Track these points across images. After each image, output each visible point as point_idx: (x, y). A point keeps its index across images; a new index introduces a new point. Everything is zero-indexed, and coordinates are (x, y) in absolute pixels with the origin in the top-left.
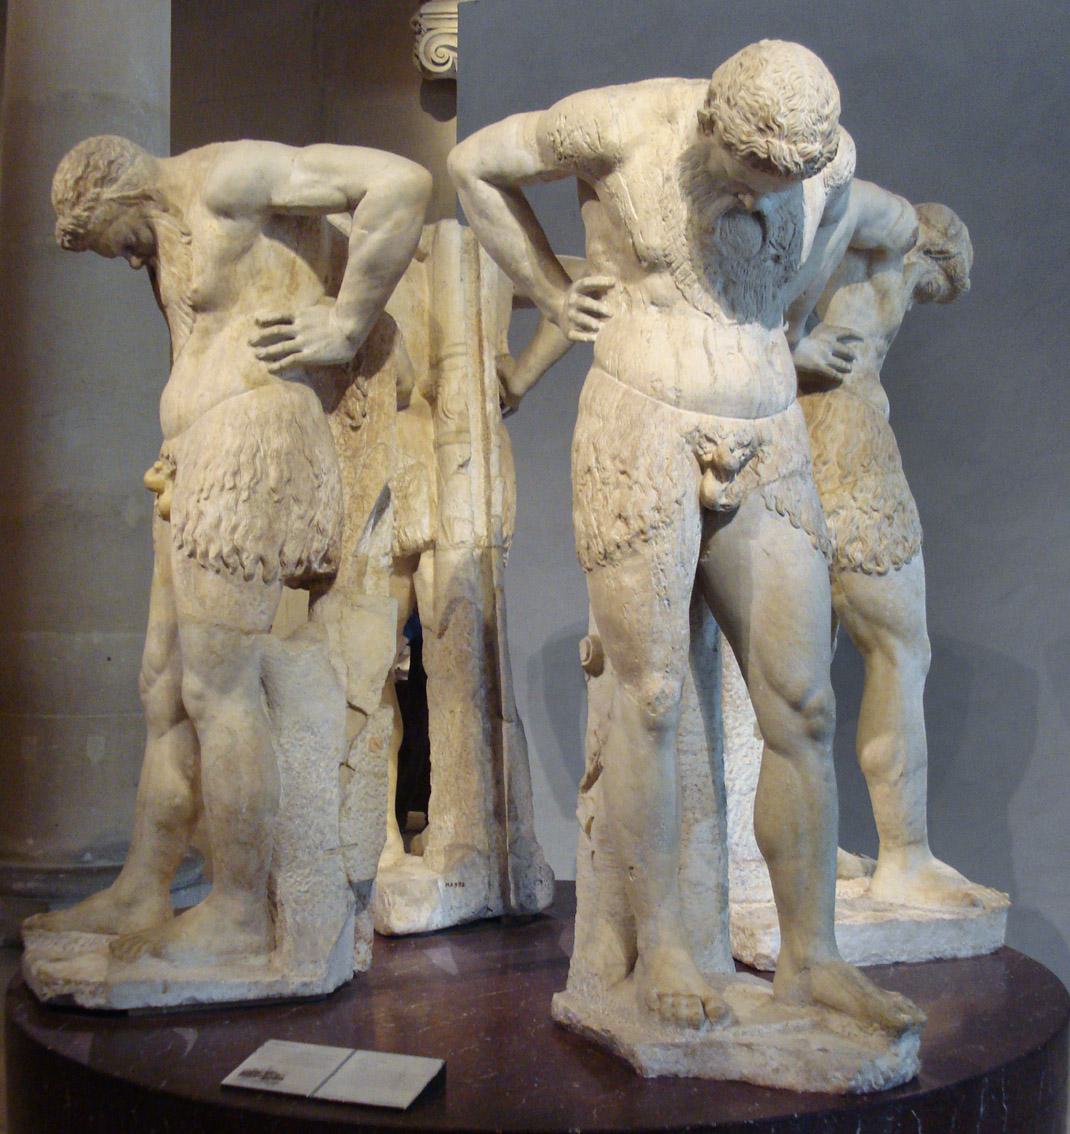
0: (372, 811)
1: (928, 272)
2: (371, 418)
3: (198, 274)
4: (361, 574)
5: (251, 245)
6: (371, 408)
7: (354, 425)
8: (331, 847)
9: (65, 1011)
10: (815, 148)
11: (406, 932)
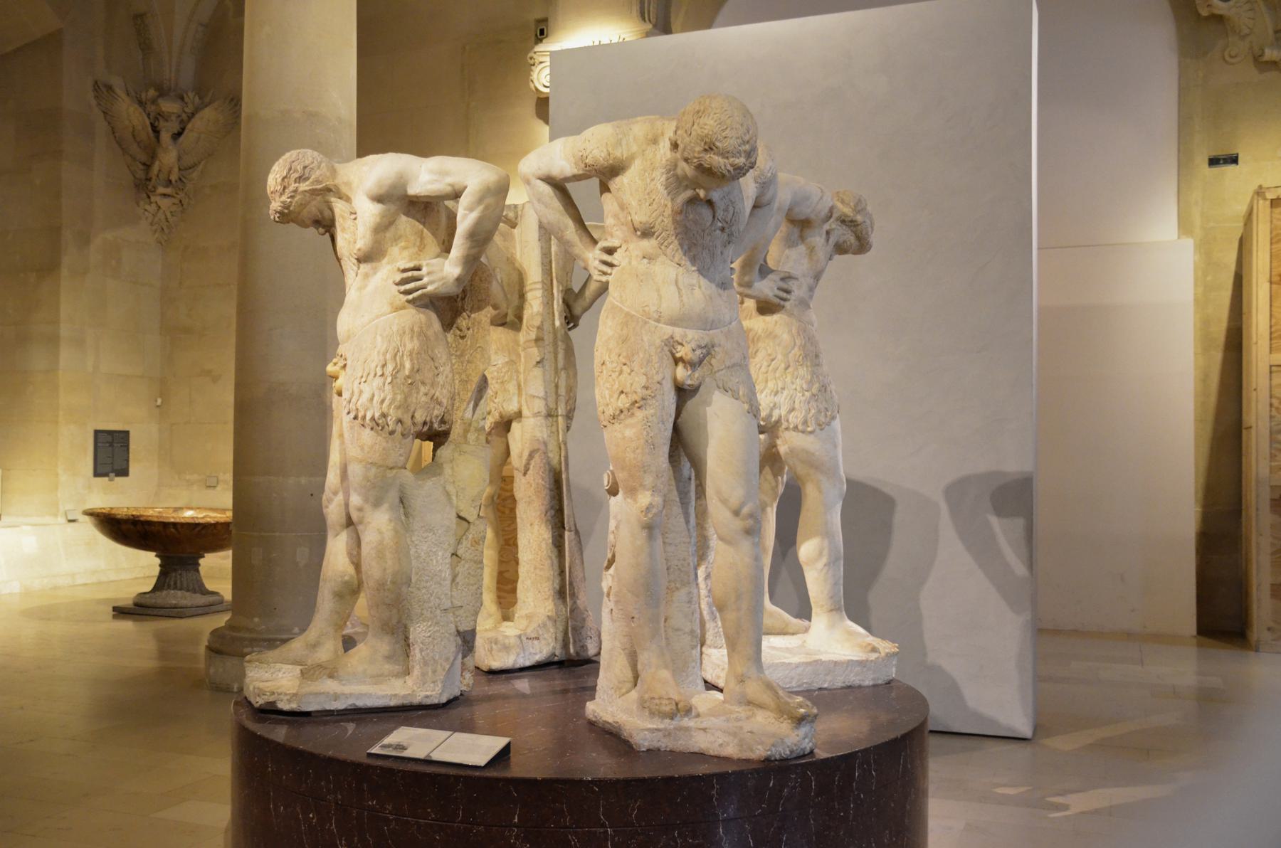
0: (472, 585)
1: (844, 234)
2: (473, 331)
3: (361, 239)
4: (466, 431)
5: (394, 221)
6: (473, 324)
7: (462, 335)
8: (445, 608)
9: (269, 712)
10: (741, 161)
11: (499, 669)
